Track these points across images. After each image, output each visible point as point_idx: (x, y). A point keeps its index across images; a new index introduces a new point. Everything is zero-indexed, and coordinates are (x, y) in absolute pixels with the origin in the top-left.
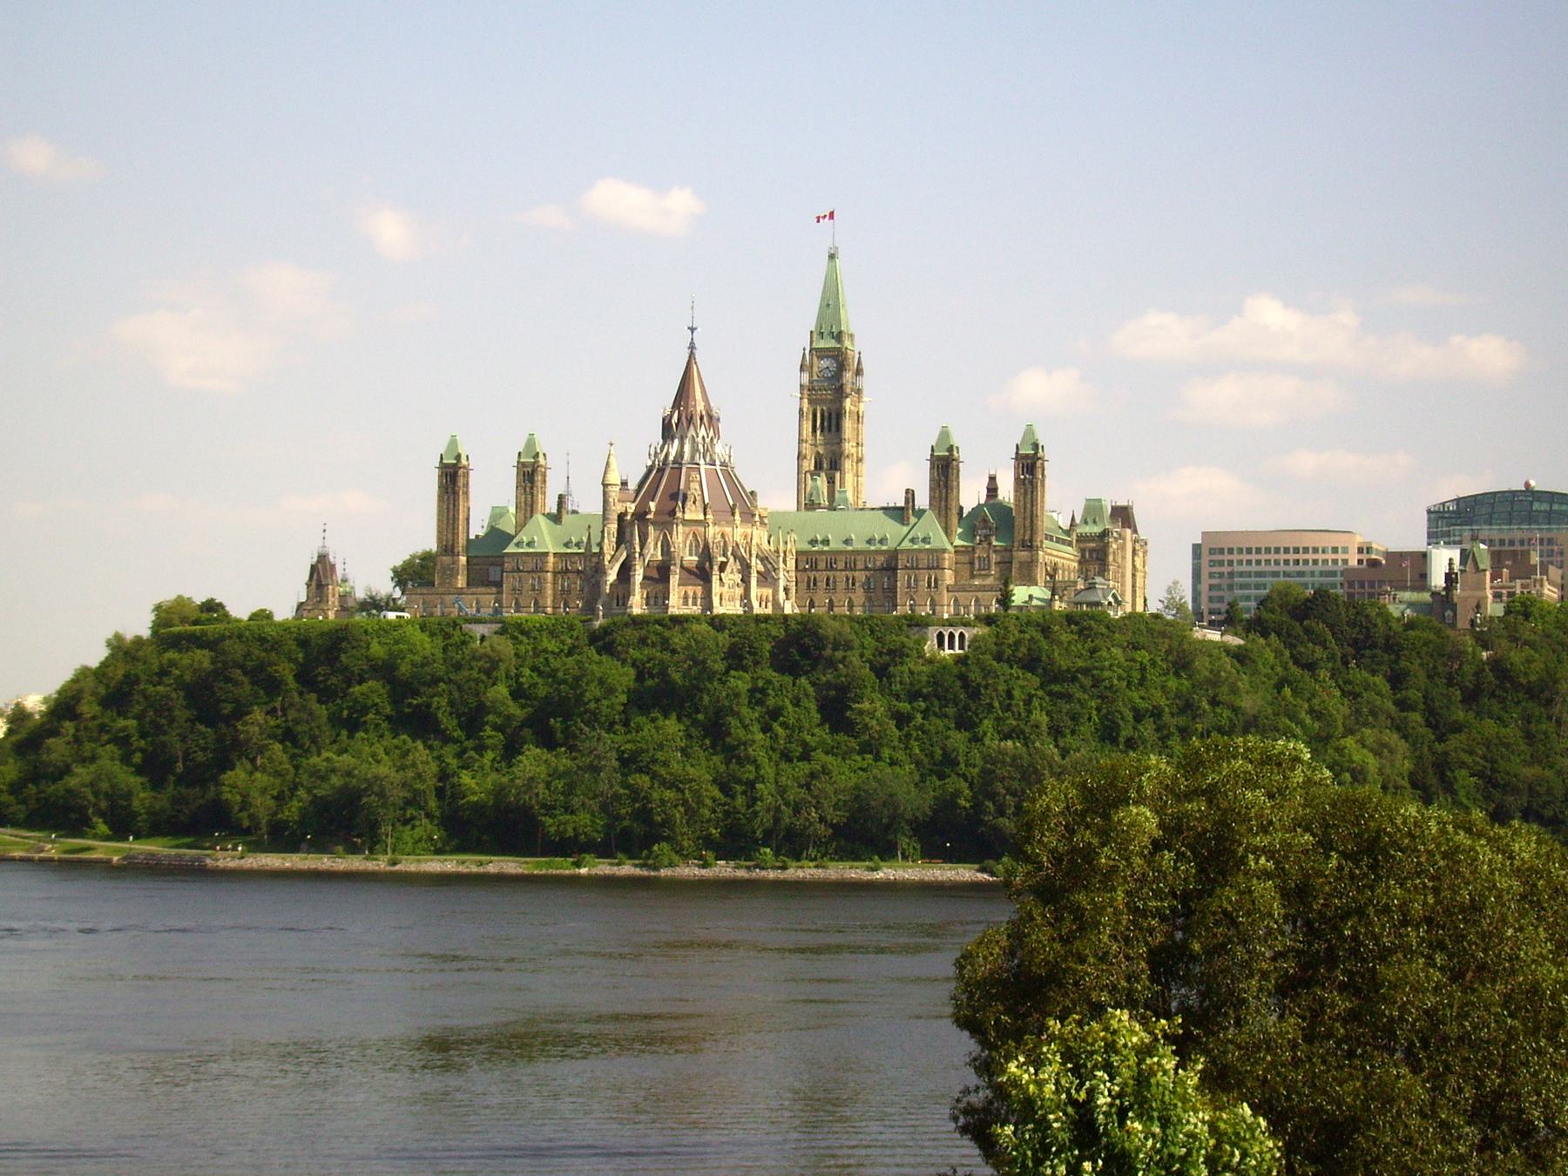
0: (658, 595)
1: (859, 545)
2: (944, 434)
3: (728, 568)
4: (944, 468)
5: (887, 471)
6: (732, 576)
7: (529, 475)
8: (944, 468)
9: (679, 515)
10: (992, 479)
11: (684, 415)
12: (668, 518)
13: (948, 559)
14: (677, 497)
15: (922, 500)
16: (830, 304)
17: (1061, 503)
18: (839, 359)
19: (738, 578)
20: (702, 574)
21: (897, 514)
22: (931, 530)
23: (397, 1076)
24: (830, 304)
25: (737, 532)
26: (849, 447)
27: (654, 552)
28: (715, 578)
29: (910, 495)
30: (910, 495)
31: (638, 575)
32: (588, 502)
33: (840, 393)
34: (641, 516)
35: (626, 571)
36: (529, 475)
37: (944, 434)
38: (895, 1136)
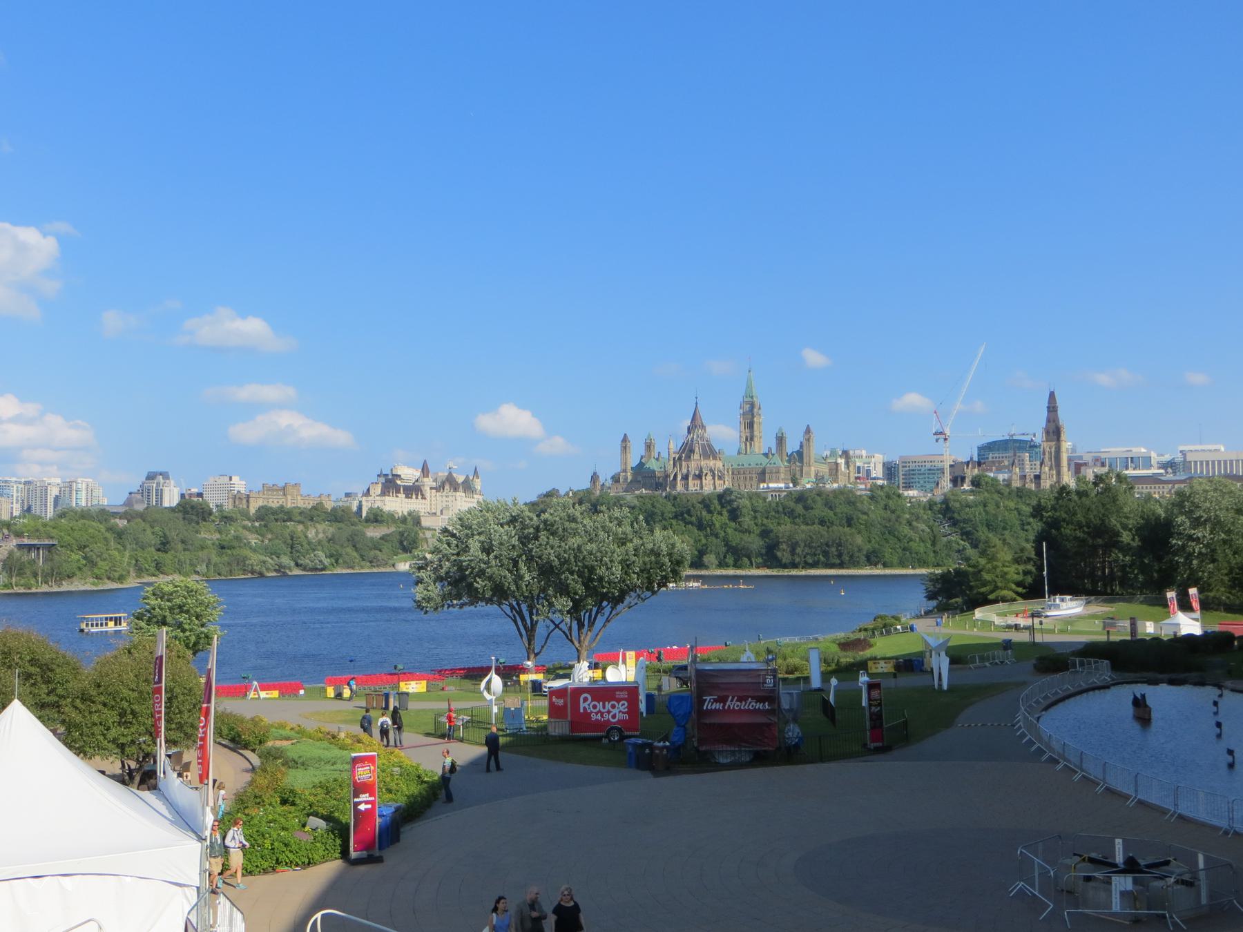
0: (686, 486)
1: (753, 465)
2: (780, 429)
4: (780, 440)
5: (764, 441)
6: (709, 477)
7: (649, 446)
8: (780, 440)
10: (1052, 395)
11: (696, 423)
12: (688, 458)
13: (782, 470)
14: (692, 451)
15: (774, 451)
16: (749, 387)
17: (818, 449)
18: (752, 405)
20: (699, 477)
21: (766, 455)
22: (776, 459)
23: (790, 661)
24: (749, 387)
25: (711, 463)
26: (756, 433)
27: (684, 471)
29: (770, 449)
30: (770, 449)
31: (679, 478)
32: (665, 455)
33: (753, 416)
34: (680, 458)
35: (675, 476)
36: (649, 446)
37: (780, 429)
38: (153, 579)
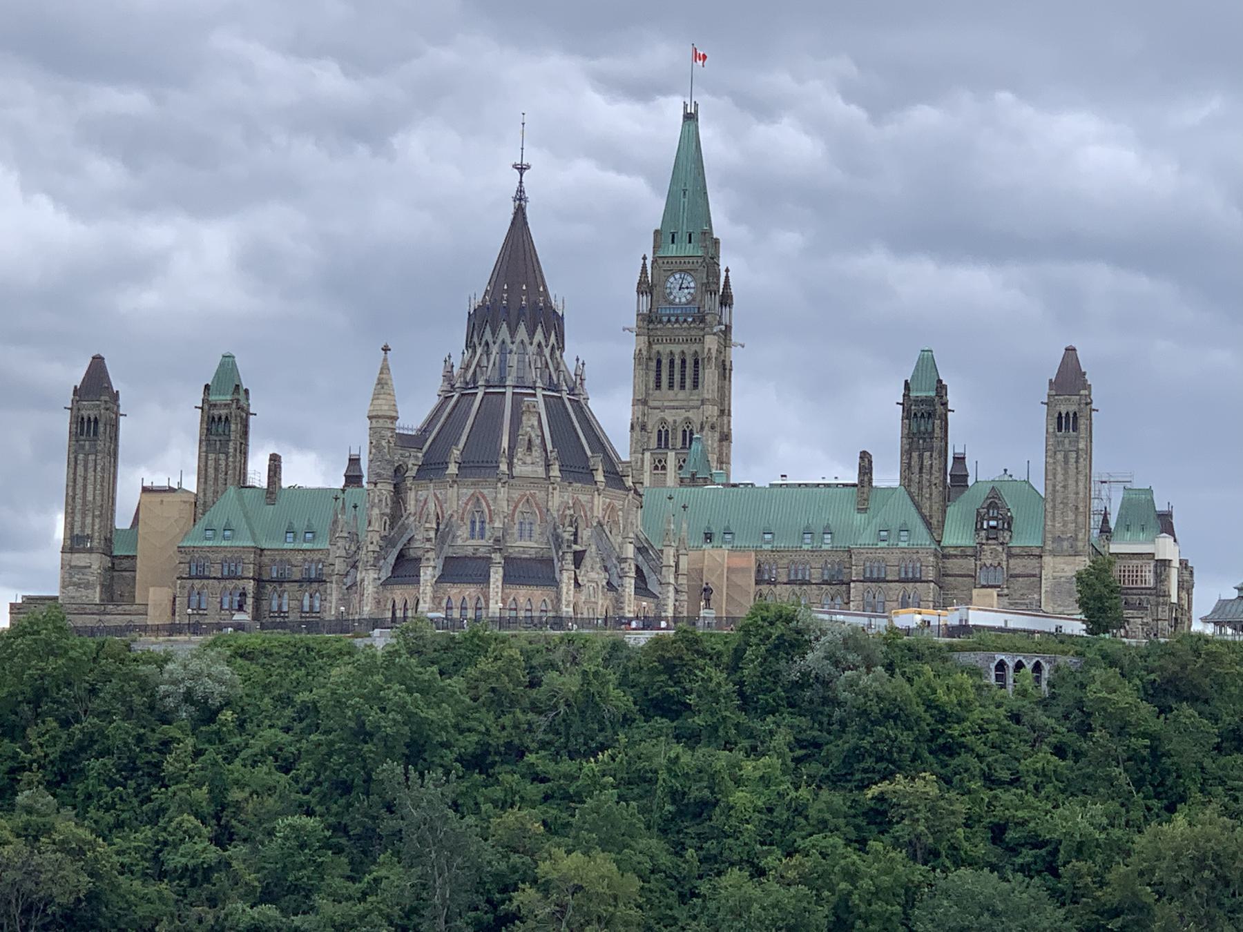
3: (587, 561)
6: (593, 575)
9: (504, 467)
19: (601, 577)
28: (566, 578)
